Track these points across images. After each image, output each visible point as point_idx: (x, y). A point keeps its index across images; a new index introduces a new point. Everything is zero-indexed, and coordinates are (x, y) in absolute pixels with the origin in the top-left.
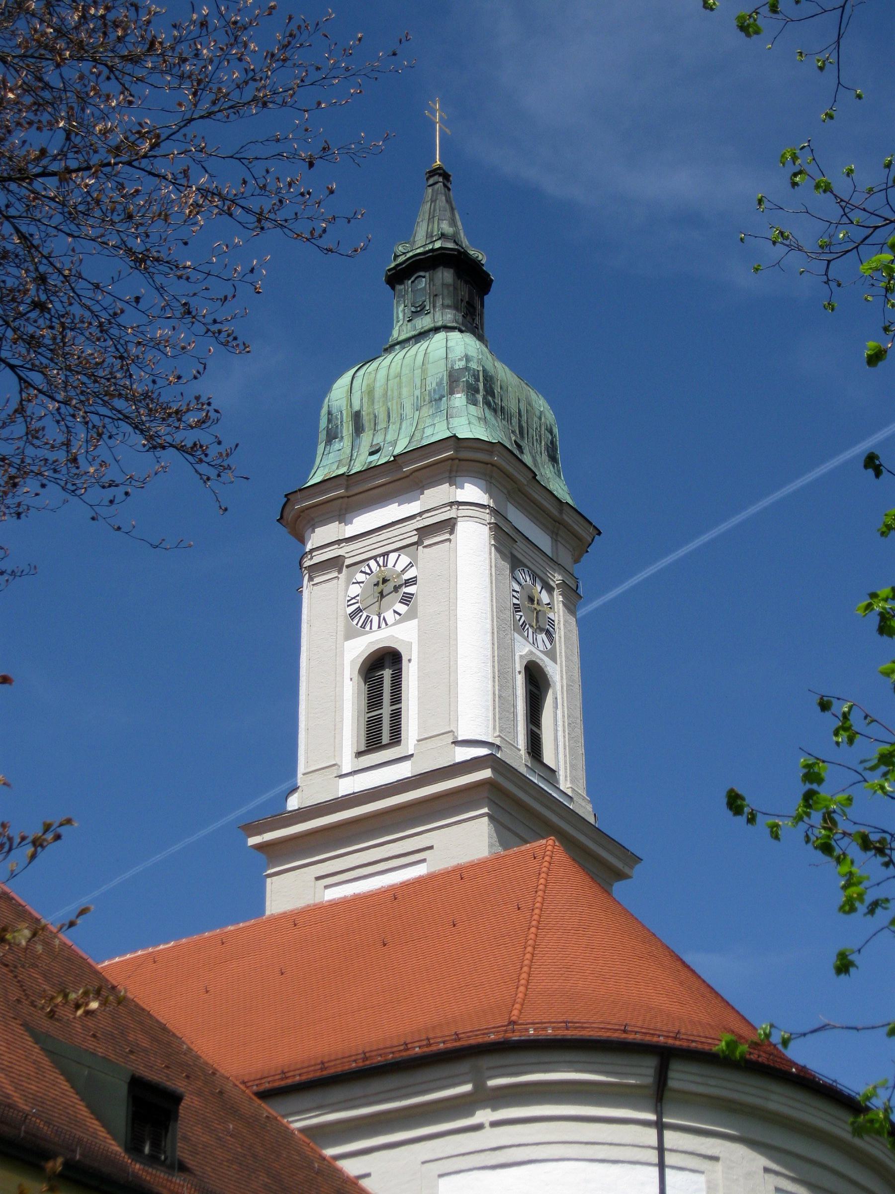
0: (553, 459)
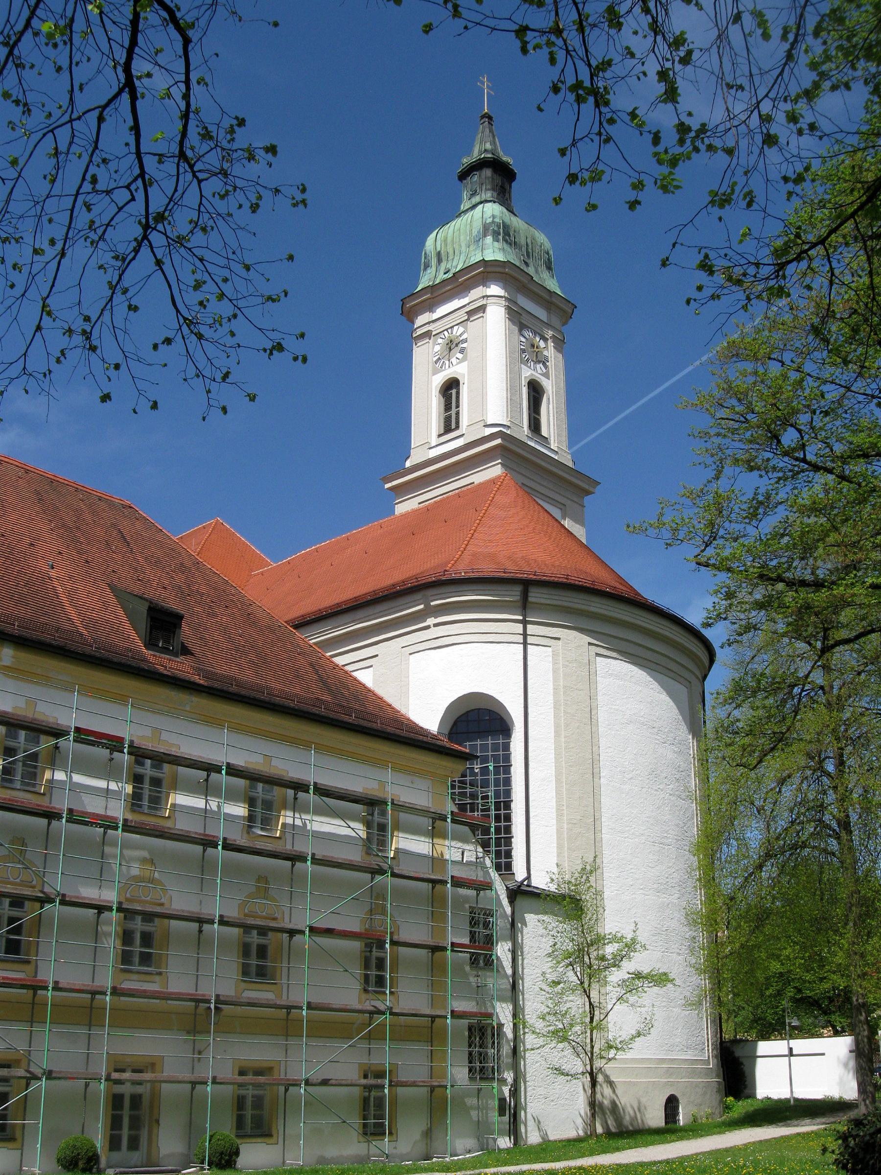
0: (549, 268)
